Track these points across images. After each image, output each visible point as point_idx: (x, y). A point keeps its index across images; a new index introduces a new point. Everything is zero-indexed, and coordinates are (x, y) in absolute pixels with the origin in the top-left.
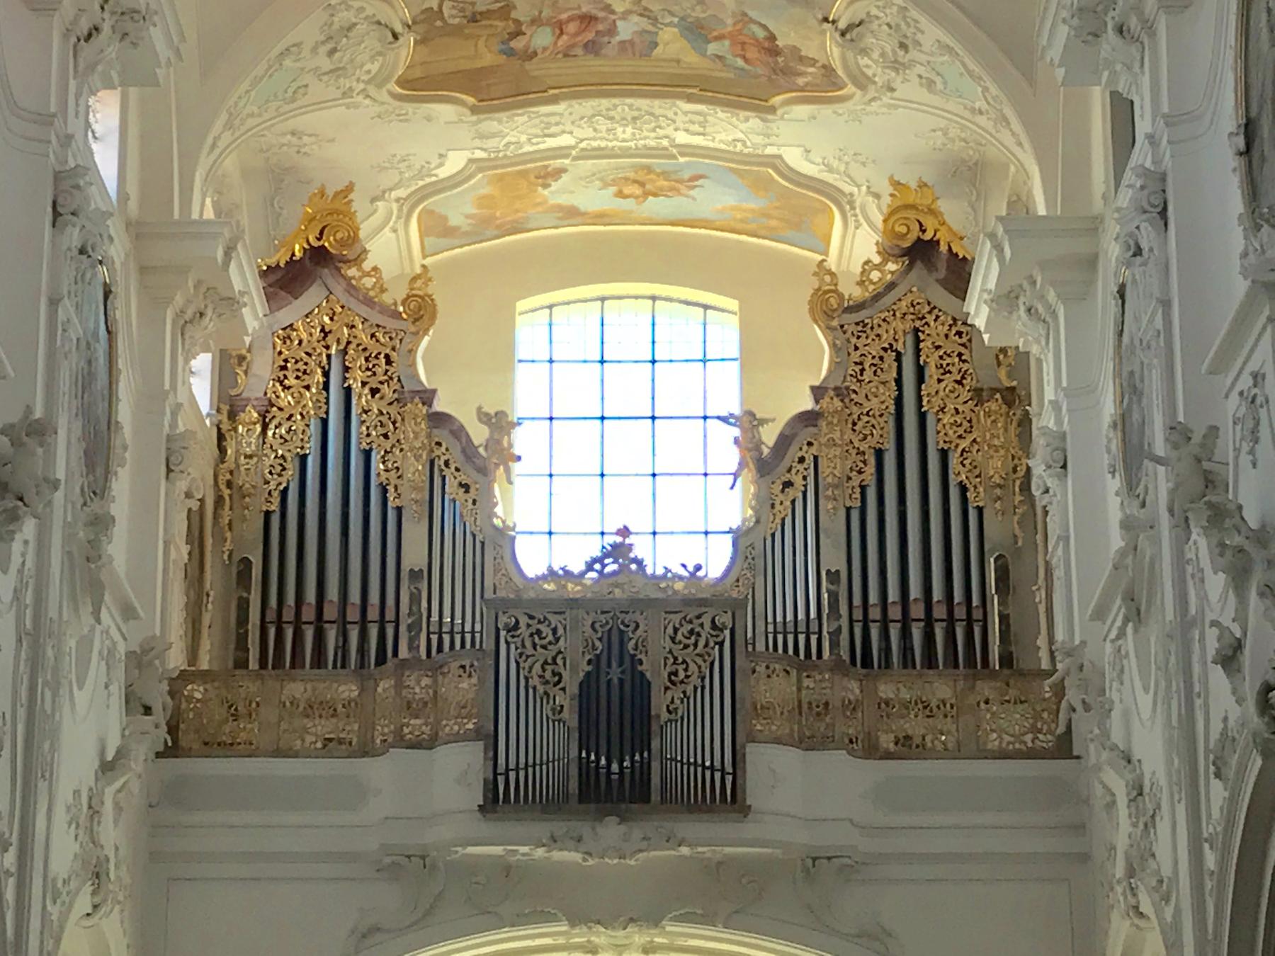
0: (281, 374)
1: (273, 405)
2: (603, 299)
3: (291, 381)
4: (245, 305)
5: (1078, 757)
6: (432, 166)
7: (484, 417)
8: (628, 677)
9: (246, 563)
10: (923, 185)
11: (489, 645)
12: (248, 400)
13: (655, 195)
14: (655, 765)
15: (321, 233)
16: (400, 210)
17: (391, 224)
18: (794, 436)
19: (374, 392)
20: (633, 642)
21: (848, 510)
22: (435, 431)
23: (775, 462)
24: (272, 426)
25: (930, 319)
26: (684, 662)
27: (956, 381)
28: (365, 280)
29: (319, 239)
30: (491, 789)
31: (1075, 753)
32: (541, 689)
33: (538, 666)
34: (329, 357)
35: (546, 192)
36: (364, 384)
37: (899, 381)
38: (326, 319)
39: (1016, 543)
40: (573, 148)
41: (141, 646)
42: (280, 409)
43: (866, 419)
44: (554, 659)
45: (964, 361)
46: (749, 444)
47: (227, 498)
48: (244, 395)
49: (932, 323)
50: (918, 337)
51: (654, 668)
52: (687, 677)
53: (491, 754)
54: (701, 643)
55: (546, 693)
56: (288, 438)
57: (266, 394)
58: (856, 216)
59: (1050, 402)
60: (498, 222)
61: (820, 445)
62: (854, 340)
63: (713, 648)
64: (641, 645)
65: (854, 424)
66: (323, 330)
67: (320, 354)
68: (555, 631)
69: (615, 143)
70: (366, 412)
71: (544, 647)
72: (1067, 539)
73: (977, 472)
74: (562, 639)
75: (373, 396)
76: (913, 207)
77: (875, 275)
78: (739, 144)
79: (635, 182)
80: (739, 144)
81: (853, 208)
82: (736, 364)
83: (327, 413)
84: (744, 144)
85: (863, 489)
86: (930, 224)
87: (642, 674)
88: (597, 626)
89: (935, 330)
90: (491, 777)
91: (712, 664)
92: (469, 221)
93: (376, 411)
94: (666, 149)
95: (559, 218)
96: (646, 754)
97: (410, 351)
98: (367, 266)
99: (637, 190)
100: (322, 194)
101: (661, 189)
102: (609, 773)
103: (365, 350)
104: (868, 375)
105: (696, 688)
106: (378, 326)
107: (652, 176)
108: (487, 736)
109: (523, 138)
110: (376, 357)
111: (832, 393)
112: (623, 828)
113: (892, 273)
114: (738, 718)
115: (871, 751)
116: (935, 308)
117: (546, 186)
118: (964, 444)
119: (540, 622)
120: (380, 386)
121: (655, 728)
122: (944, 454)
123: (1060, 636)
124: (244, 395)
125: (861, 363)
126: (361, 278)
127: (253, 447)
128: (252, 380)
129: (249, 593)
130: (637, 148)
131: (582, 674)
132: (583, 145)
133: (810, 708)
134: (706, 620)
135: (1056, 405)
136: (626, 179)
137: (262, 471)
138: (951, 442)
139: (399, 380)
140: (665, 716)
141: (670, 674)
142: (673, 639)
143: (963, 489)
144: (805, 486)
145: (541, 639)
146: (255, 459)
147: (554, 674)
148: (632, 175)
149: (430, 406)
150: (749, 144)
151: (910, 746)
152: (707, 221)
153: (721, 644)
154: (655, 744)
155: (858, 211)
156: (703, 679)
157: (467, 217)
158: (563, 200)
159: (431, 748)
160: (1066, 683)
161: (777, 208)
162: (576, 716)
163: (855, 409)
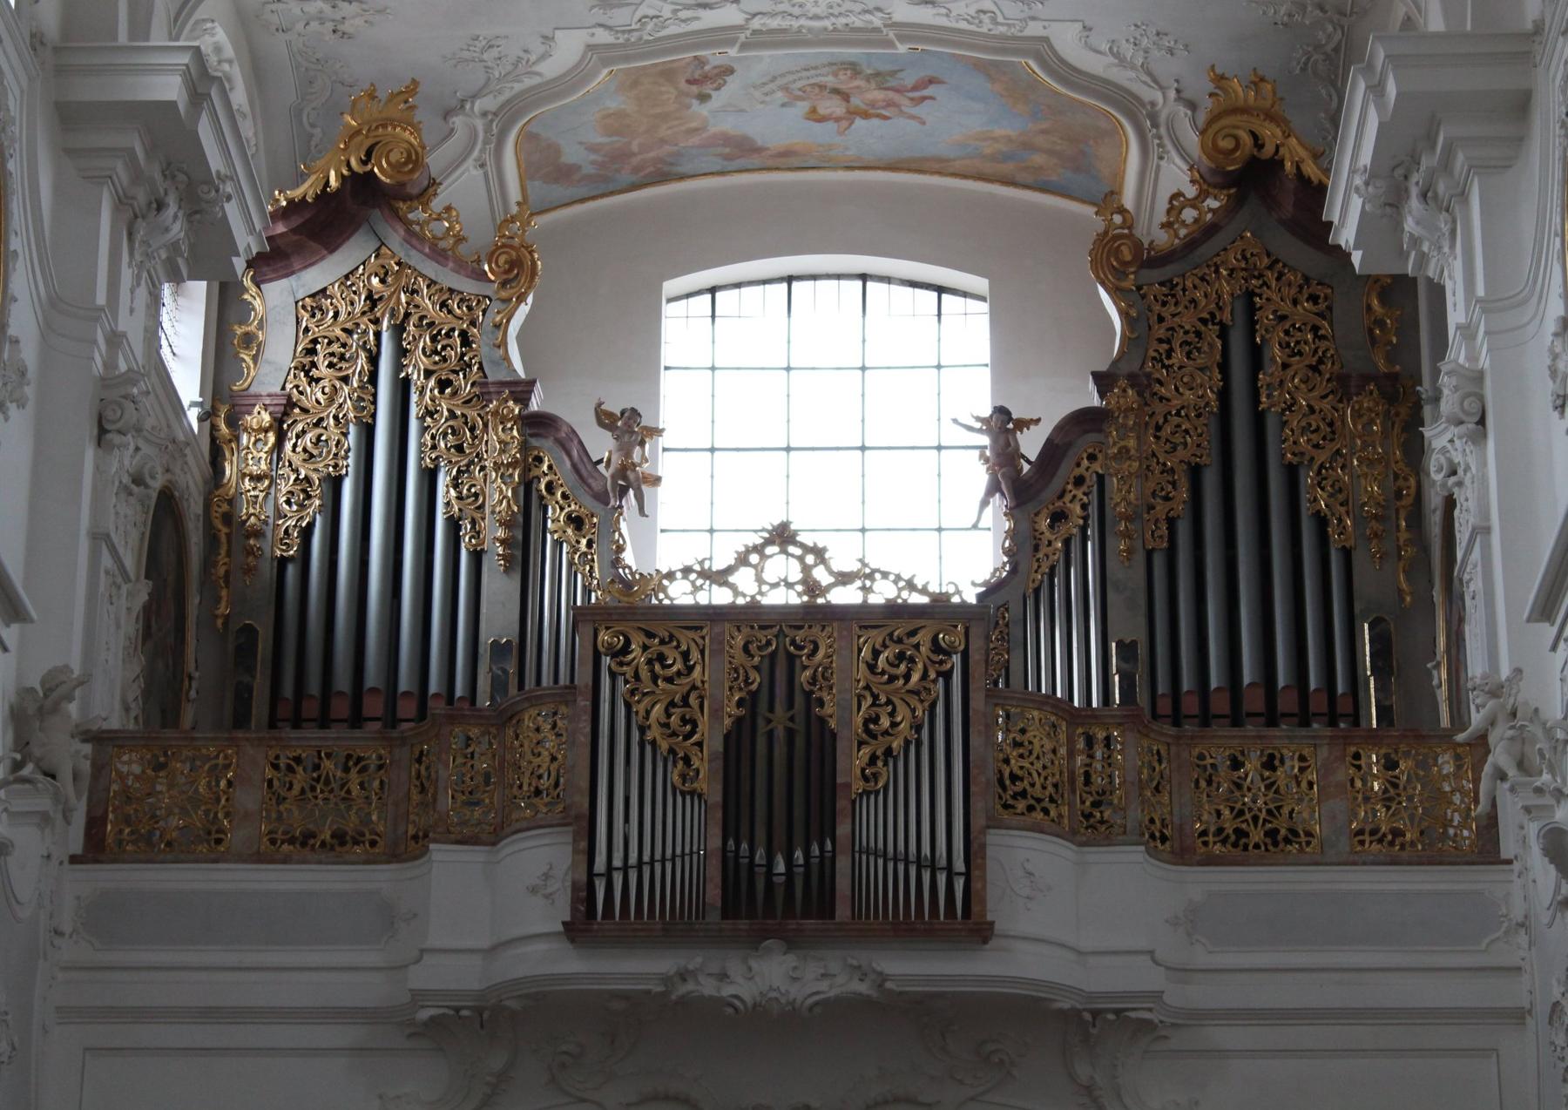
0: (307, 360)
1: (295, 405)
2: (790, 279)
3: (323, 370)
4: (229, 198)
5: (1509, 862)
6: (533, 58)
7: (605, 419)
8: (799, 725)
9: (249, 632)
10: (1258, 81)
11: (584, 677)
12: (258, 396)
13: (866, 115)
14: (843, 864)
15: (369, 153)
16: (488, 130)
17: (476, 154)
18: (1069, 445)
19: (443, 385)
20: (808, 673)
21: (1149, 554)
22: (534, 442)
23: (1034, 483)
24: (292, 435)
25: (1270, 276)
26: (889, 702)
27: (1310, 367)
28: (433, 225)
29: (365, 163)
30: (584, 896)
31: (1504, 855)
32: (664, 745)
33: (658, 710)
34: (378, 335)
35: (703, 110)
36: (428, 374)
37: (1224, 368)
38: (375, 281)
39: (1403, 600)
40: (741, 28)
41: (43, 683)
42: (305, 411)
43: (1177, 420)
44: (685, 699)
45: (1323, 337)
46: (1004, 458)
47: (223, 539)
48: (253, 390)
49: (1274, 283)
50: (1254, 304)
51: (842, 710)
52: (894, 725)
53: (584, 844)
54: (915, 677)
55: (672, 751)
56: (315, 452)
57: (283, 388)
58: (1160, 138)
59: (1458, 327)
60: (635, 161)
61: (1106, 456)
62: (1157, 308)
63: (935, 681)
64: (823, 676)
65: (1158, 428)
66: (369, 297)
67: (365, 332)
68: (686, 656)
69: (803, 22)
70: (430, 414)
71: (669, 680)
72: (1487, 530)
73: (1341, 497)
74: (698, 668)
75: (442, 392)
76: (1244, 110)
77: (1189, 215)
78: (986, 18)
79: (836, 91)
80: (986, 18)
81: (1155, 125)
82: (988, 370)
83: (374, 416)
84: (994, 21)
85: (1171, 522)
86: (1270, 132)
87: (822, 721)
88: (753, 648)
89: (1274, 300)
90: (584, 878)
91: (933, 705)
92: (593, 157)
93: (446, 413)
94: (877, 30)
95: (727, 158)
96: (829, 846)
97: (497, 326)
98: (437, 204)
99: (834, 106)
100: (372, 96)
101: (873, 104)
102: (770, 872)
103: (431, 324)
104: (1178, 356)
105: (907, 743)
106: (451, 291)
107: (857, 83)
108: (578, 817)
109: (667, 11)
110: (448, 335)
111: (1123, 383)
112: (791, 960)
113: (1214, 211)
114: (973, 789)
115: (1171, 844)
116: (1277, 261)
117: (703, 98)
118: (1322, 457)
119: (662, 642)
120: (452, 377)
121: (842, 804)
122: (1292, 474)
123: (1476, 667)
124: (253, 390)
125: (1168, 341)
126: (427, 222)
127: (263, 466)
128: (264, 368)
129: (254, 677)
130: (835, 30)
131: (727, 722)
132: (756, 24)
133: (1087, 782)
134: (923, 638)
135: (1468, 331)
136: (822, 87)
137: (276, 498)
138: (1302, 454)
139: (481, 368)
140: (859, 786)
141: (866, 722)
142: (872, 667)
143: (1321, 521)
144: (1085, 519)
145: (665, 667)
146: (267, 482)
147: (684, 721)
148: (830, 80)
149: (527, 406)
150: (1000, 19)
151: (1246, 848)
152: (940, 160)
153: (947, 676)
154: (843, 829)
155: (1163, 131)
156: (918, 729)
157: (592, 149)
158: (728, 125)
159: (494, 844)
160: (1492, 740)
161: (1043, 132)
162: (719, 787)
163: (1160, 408)
